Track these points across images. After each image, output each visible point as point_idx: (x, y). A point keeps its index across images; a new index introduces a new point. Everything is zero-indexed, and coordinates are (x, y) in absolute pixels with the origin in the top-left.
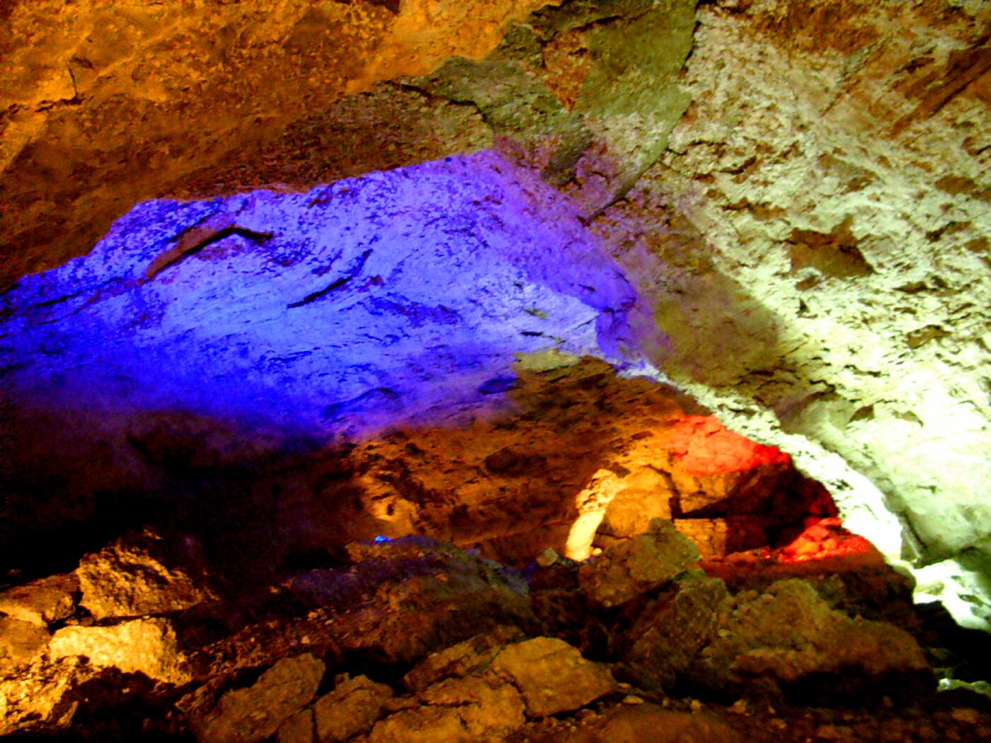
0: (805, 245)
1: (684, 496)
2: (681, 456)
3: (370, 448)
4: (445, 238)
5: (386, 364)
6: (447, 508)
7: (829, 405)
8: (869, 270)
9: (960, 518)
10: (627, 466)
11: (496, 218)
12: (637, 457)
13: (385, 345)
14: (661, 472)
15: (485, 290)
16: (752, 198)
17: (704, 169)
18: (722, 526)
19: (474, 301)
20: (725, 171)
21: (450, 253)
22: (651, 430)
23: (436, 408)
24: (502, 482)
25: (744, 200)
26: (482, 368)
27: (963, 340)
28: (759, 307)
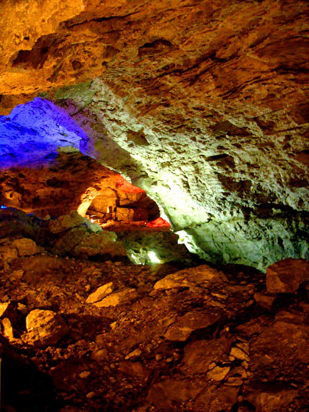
0: (131, 133)
1: (121, 199)
2: (121, 185)
3: (6, 173)
4: (32, 109)
5: (12, 145)
6: (32, 197)
7: (145, 179)
8: (148, 144)
9: (182, 219)
10: (100, 187)
11: (48, 105)
12: (104, 184)
13: (12, 139)
14: (113, 190)
15: (46, 125)
16: (116, 118)
17: (103, 108)
18: (132, 211)
19: (43, 129)
20: (109, 110)
21: (34, 114)
22: (109, 175)
23: (30, 161)
24: (52, 189)
25: (114, 118)
26: (46, 150)
27: (175, 167)
28: (120, 147)
